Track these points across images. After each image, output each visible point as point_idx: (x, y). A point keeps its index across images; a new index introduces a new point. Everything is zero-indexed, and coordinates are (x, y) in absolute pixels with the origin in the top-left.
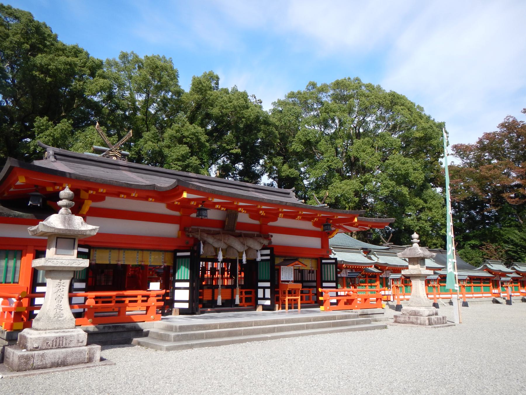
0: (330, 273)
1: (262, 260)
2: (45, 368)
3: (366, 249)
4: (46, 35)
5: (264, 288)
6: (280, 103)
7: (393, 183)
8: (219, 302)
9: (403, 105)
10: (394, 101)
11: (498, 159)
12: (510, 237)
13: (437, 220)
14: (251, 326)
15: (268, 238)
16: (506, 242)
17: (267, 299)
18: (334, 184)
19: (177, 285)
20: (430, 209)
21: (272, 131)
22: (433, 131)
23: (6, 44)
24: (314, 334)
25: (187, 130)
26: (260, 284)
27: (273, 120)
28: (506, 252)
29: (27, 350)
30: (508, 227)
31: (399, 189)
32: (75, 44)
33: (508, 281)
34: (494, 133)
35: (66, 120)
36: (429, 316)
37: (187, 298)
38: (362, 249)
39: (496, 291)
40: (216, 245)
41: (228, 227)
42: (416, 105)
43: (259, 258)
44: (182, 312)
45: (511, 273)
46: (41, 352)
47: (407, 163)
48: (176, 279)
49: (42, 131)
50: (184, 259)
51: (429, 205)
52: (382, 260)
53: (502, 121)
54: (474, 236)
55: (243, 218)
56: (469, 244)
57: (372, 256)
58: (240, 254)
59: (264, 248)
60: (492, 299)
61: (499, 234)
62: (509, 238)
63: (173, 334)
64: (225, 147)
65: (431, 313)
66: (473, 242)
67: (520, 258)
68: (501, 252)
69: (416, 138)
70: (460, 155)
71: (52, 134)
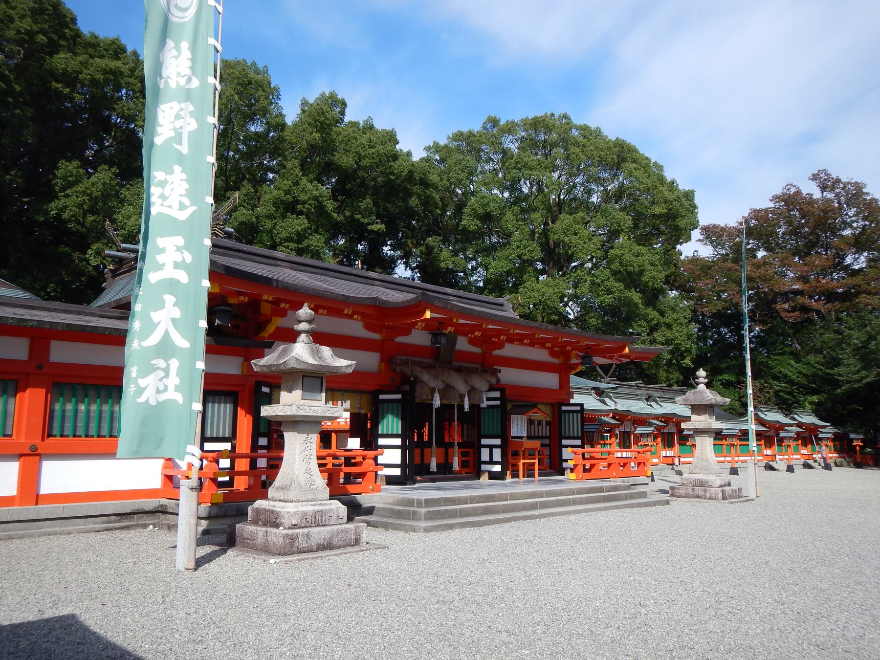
0: (574, 424)
1: (489, 407)
2: (310, 551)
3: (598, 389)
4: (68, 20)
5: (491, 447)
6: (436, 148)
7: (620, 285)
8: (433, 467)
9: (634, 162)
10: (621, 156)
11: (767, 249)
12: (783, 370)
13: (680, 344)
14: (507, 500)
15: (495, 373)
16: (776, 378)
17: (496, 463)
18: (527, 284)
19: (382, 441)
20: (669, 326)
21: (430, 196)
22: (681, 205)
23: (11, 34)
24: (587, 511)
25: (304, 191)
26: (484, 441)
27: (433, 178)
28: (776, 393)
29: (285, 528)
30: (779, 354)
31: (627, 294)
32: (115, 37)
33: (791, 438)
34: (766, 210)
35: (106, 167)
36: (721, 487)
37: (399, 462)
38: (593, 388)
39: (769, 452)
40: (432, 384)
41: (441, 356)
42: (653, 161)
43: (484, 405)
44: (391, 480)
45: (791, 425)
46: (306, 530)
47: (643, 255)
48: (380, 432)
49: (71, 185)
50: (390, 405)
51: (667, 320)
52: (623, 405)
53: (778, 191)
54: (727, 368)
55: (462, 344)
56: (720, 380)
57: (607, 400)
58: (462, 397)
59: (491, 389)
60: (802, 461)
61: (767, 366)
62: (781, 372)
63: (423, 510)
64: (358, 219)
65: (723, 483)
66: (726, 377)
67: (797, 402)
68: (768, 393)
69: (655, 215)
70: (711, 242)
71: (88, 192)
